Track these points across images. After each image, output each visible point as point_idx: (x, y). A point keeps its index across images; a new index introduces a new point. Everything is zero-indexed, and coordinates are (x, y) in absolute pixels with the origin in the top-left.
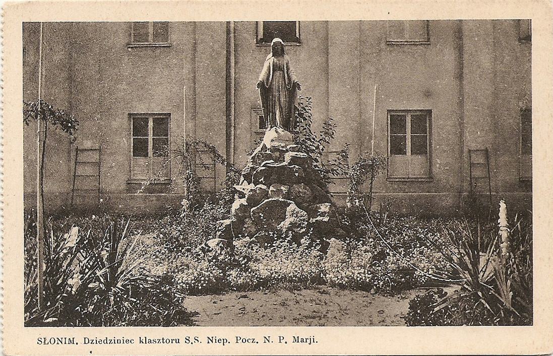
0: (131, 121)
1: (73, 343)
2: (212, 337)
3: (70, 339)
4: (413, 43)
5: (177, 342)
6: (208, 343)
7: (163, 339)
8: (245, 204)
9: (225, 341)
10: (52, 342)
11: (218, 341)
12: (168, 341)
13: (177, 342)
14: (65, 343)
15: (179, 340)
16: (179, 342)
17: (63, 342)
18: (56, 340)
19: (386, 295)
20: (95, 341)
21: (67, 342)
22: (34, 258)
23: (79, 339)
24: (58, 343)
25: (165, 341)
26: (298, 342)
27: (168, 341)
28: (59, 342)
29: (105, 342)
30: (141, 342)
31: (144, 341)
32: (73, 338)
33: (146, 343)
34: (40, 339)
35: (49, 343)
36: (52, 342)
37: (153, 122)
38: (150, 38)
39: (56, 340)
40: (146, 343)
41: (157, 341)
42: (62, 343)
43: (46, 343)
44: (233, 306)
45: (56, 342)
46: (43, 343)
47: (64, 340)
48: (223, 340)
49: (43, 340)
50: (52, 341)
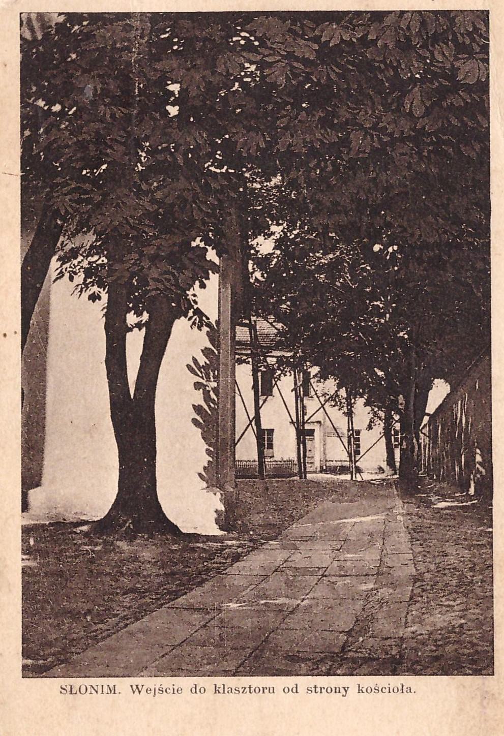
1: (114, 693)
3: (108, 686)
4: (349, 110)
5: (271, 691)
6: (348, 688)
7: (250, 687)
8: (169, 106)
9: (194, 690)
11: (178, 690)
12: (257, 690)
13: (271, 691)
14: (102, 693)
15: (273, 688)
16: (273, 692)
17: (100, 691)
20: (247, 690)
22: (166, 630)
23: (279, 688)
24: (91, 693)
25: (252, 690)
27: (257, 690)
28: (93, 692)
29: (294, 690)
30: (217, 691)
31: (221, 690)
32: (143, 686)
33: (224, 693)
34: (309, 689)
35: (78, 692)
40: (224, 693)
41: (241, 691)
42: (97, 692)
43: (74, 691)
47: (100, 687)
48: (196, 692)
49: (68, 689)
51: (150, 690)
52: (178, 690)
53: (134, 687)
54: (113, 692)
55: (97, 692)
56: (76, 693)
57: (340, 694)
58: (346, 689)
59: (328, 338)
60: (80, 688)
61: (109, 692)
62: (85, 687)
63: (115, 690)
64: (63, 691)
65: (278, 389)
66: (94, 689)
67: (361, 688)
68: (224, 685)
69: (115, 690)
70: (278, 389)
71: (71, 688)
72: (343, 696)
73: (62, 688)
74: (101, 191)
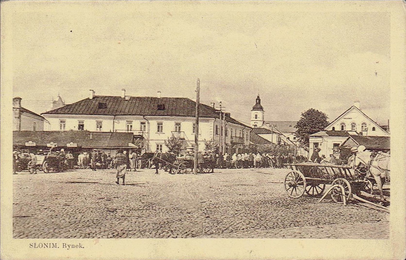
0: (403, 7)
2: (47, 244)
3: (53, 244)
10: (41, 246)
11: (76, 246)
14: (50, 247)
18: (43, 245)
19: (45, 153)
21: (51, 246)
24: (44, 248)
26: (56, 247)
28: (45, 246)
32: (56, 244)
35: (38, 247)
36: (41, 246)
37: (211, 107)
38: (160, 127)
39: (43, 245)
43: (36, 247)
44: (185, 180)
45: (43, 247)
46: (34, 247)
49: (34, 245)
50: (41, 245)
51: (78, 246)
52: (76, 246)
53: (64, 244)
54: (55, 247)
55: (47, 247)
56: (37, 247)
57: (66, 249)
58: (69, 246)
59: (144, 164)
60: (39, 245)
61: (53, 247)
62: (41, 244)
63: (56, 246)
64: (31, 246)
65: (349, 131)
66: (46, 246)
67: (81, 245)
68: (80, 244)
69: (56, 246)
70: (349, 131)
71: (35, 245)
72: (68, 249)
73: (31, 245)
74: (160, 167)
